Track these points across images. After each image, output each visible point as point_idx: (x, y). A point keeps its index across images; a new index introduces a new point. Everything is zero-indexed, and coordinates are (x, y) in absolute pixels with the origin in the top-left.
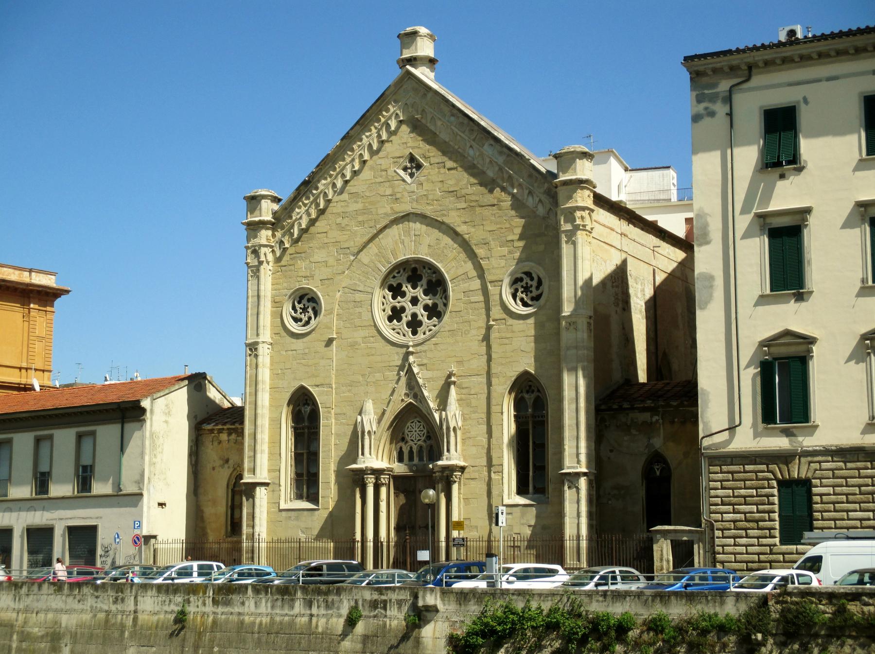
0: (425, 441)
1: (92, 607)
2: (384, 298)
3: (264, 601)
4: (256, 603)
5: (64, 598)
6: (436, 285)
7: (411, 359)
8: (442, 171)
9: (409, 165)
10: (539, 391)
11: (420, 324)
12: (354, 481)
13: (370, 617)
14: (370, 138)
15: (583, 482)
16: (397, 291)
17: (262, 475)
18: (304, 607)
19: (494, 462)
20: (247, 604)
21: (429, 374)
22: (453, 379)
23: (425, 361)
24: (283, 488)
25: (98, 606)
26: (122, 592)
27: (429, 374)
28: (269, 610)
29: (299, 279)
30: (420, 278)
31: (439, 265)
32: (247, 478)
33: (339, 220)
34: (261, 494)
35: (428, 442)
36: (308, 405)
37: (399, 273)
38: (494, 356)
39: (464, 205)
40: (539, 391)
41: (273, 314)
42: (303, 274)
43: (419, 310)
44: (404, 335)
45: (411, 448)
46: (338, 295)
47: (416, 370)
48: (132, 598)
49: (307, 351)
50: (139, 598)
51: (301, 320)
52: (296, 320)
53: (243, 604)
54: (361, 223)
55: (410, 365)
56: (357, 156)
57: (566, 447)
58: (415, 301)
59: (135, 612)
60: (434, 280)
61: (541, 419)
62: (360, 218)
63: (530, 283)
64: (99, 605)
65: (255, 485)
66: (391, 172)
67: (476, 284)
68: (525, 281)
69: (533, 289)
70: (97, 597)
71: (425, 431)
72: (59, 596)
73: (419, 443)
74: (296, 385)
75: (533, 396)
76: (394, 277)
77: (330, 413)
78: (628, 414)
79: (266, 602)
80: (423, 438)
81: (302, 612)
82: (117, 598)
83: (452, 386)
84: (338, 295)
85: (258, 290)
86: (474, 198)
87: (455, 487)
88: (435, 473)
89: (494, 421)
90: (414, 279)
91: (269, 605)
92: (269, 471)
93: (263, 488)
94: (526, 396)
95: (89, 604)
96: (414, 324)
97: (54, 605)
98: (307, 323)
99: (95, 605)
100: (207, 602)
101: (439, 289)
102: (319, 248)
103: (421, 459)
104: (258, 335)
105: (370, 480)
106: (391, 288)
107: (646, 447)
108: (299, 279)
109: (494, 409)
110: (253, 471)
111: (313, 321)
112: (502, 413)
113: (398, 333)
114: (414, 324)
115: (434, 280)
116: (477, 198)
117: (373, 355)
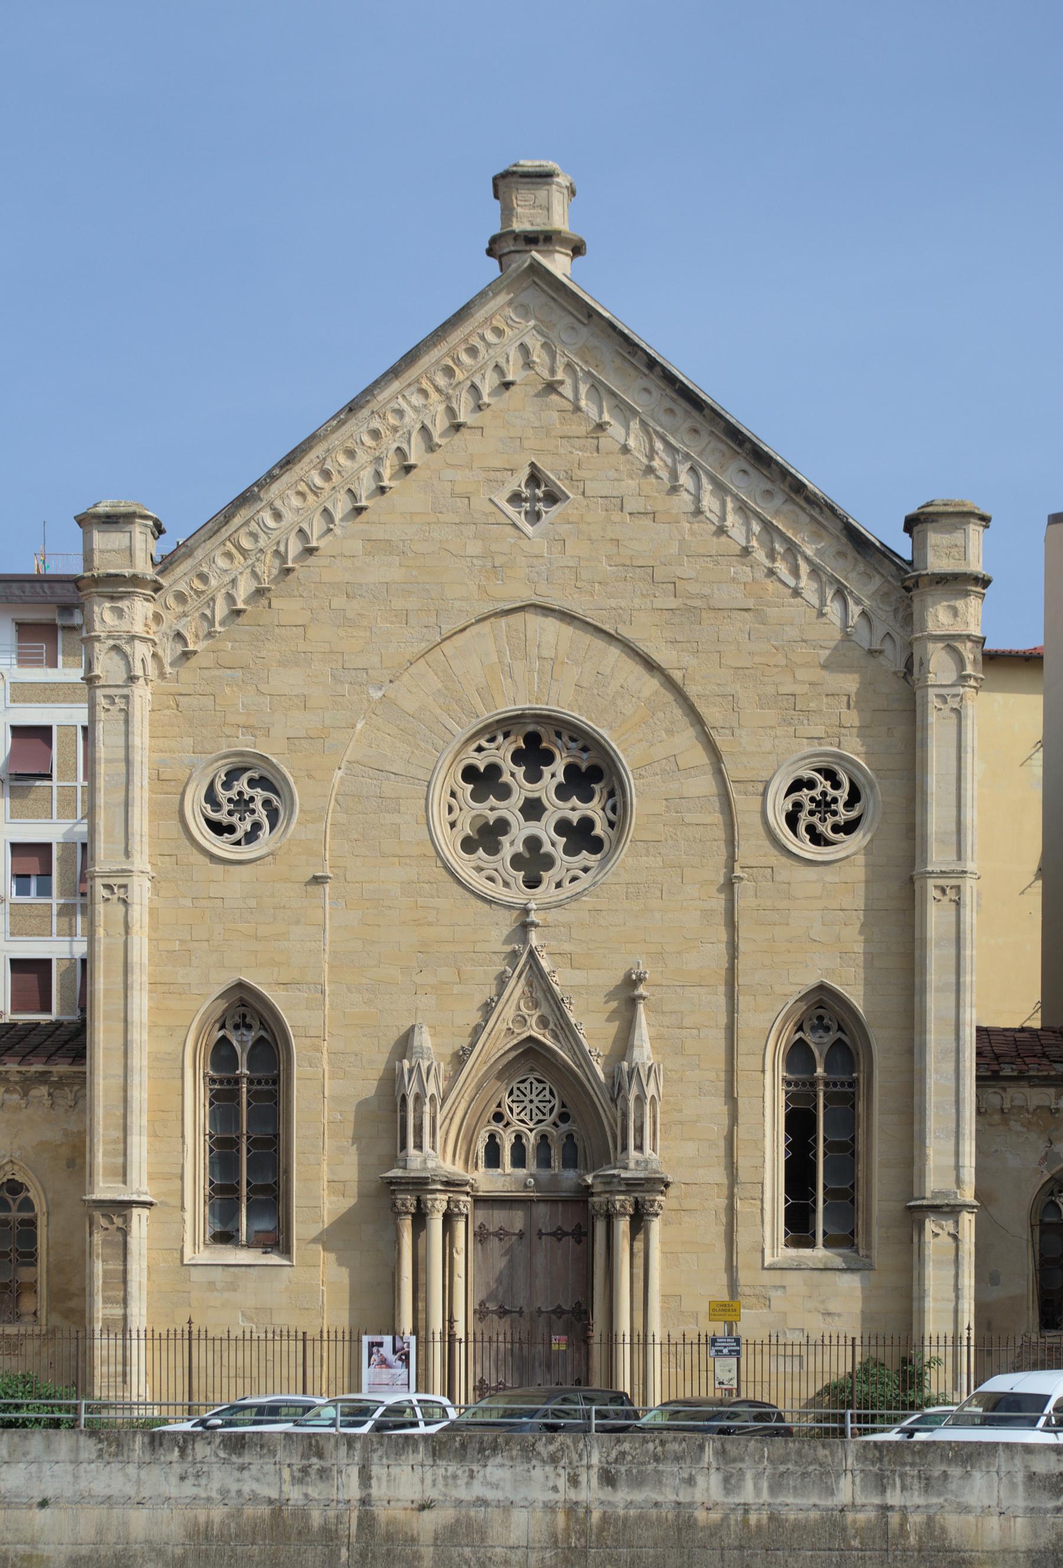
0: (555, 1124)
1: (224, 1492)
2: (453, 794)
3: (749, 1475)
4: (726, 1480)
5: (131, 1469)
6: (593, 772)
7: (534, 938)
8: (616, 516)
9: (526, 493)
10: (263, 1025)
11: (548, 862)
12: (395, 1200)
13: (1046, 1511)
14: (413, 406)
15: (968, 1222)
16: (483, 780)
17: (140, 1187)
18: (864, 1488)
19: (743, 1175)
20: (700, 1480)
21: (578, 977)
22: (641, 990)
23: (567, 947)
24: (188, 1216)
25: (246, 1489)
26: (320, 1456)
27: (578, 977)
28: (765, 1497)
29: (227, 730)
30: (548, 758)
31: (605, 733)
32: (104, 1189)
33: (338, 602)
34: (140, 1222)
35: (564, 1127)
36: (249, 1027)
37: (492, 740)
38: (742, 947)
39: (673, 603)
40: (840, 1029)
41: (156, 812)
42: (241, 720)
43: (521, 830)
44: (506, 884)
45: (518, 1137)
46: (340, 773)
47: (545, 964)
48: (354, 1471)
49: (253, 903)
50: (376, 1470)
51: (231, 829)
52: (218, 828)
53: (690, 1481)
54: (405, 617)
55: (531, 954)
56: (391, 453)
57: (930, 1152)
58: (533, 809)
59: (365, 1502)
60: (584, 766)
61: (847, 1089)
62: (398, 604)
63: (816, 793)
64: (248, 1487)
65: (125, 1206)
66: (479, 503)
67: (704, 785)
68: (820, 789)
69: (840, 807)
70: (242, 1468)
71: (556, 1102)
72: (115, 1466)
73: (541, 1127)
74: (228, 979)
75: (251, 1037)
76: (480, 749)
77: (318, 1049)
78: (1004, 1089)
79: (757, 1477)
80: (550, 1119)
81: (859, 1501)
82: (305, 1470)
83: (641, 1007)
84: (340, 773)
85: (127, 747)
86: (693, 588)
87: (656, 1226)
88: (592, 1194)
89: (742, 1091)
90: (533, 756)
91: (765, 1485)
92: (151, 1177)
93: (145, 1212)
94: (810, 1039)
95: (216, 1485)
96: (533, 864)
97: (99, 1488)
98: (251, 837)
99: (234, 1487)
100: (583, 1479)
101: (597, 787)
102: (283, 664)
103: (544, 1162)
104: (127, 854)
105: (439, 1203)
106: (470, 774)
107: (1045, 1158)
108: (227, 730)
109: (743, 1062)
110: (123, 1174)
111: (264, 833)
112: (763, 1071)
113: (491, 879)
114: (533, 864)
115: (584, 766)
116: (706, 591)
117: (430, 924)
